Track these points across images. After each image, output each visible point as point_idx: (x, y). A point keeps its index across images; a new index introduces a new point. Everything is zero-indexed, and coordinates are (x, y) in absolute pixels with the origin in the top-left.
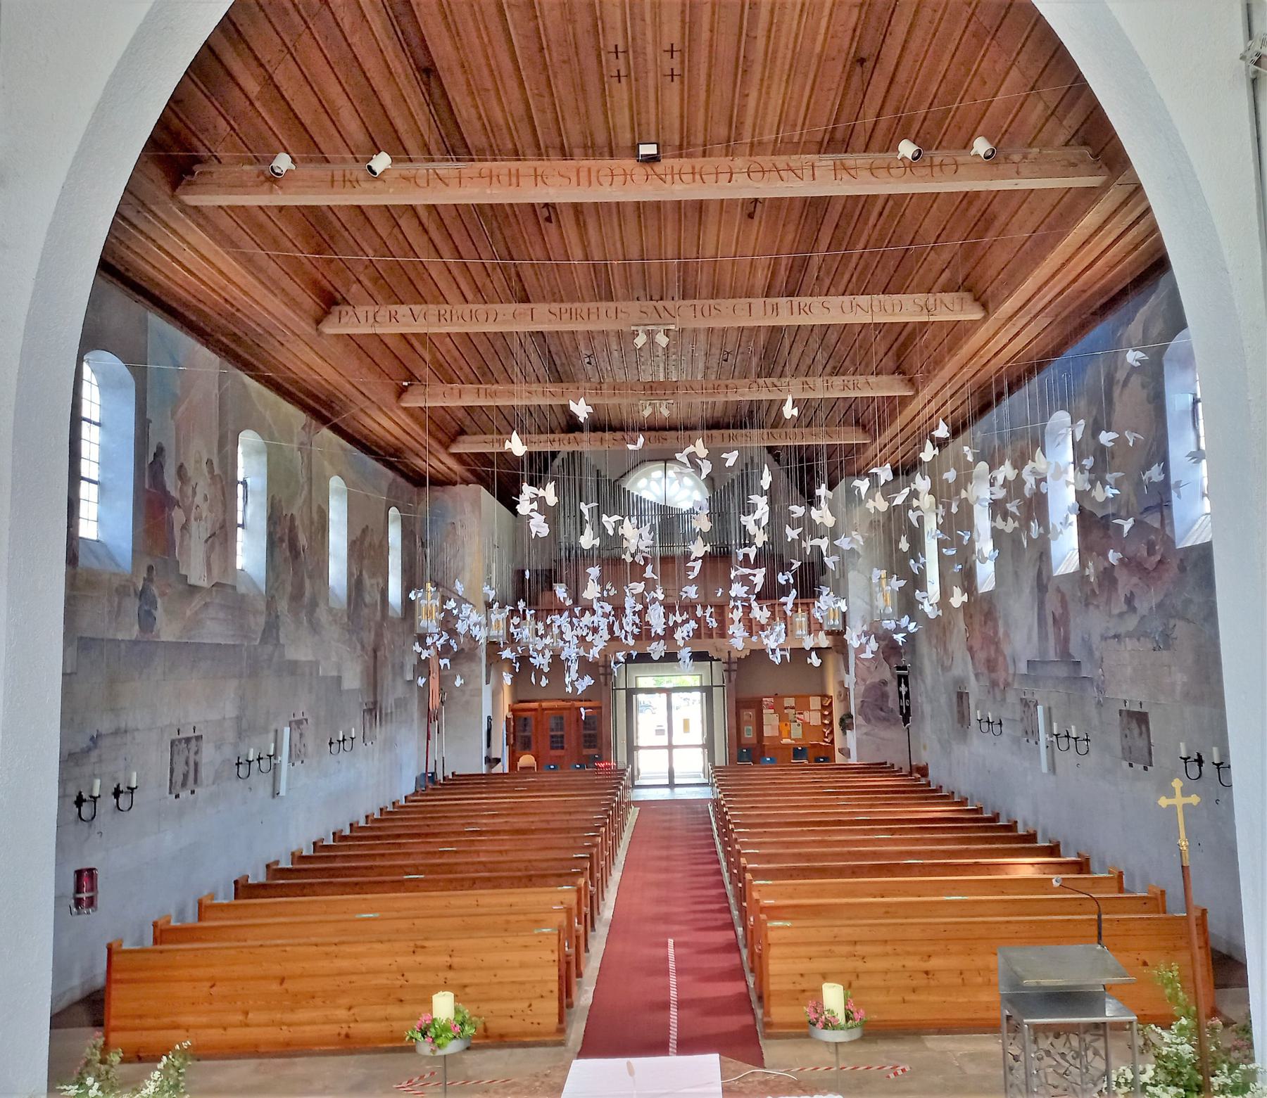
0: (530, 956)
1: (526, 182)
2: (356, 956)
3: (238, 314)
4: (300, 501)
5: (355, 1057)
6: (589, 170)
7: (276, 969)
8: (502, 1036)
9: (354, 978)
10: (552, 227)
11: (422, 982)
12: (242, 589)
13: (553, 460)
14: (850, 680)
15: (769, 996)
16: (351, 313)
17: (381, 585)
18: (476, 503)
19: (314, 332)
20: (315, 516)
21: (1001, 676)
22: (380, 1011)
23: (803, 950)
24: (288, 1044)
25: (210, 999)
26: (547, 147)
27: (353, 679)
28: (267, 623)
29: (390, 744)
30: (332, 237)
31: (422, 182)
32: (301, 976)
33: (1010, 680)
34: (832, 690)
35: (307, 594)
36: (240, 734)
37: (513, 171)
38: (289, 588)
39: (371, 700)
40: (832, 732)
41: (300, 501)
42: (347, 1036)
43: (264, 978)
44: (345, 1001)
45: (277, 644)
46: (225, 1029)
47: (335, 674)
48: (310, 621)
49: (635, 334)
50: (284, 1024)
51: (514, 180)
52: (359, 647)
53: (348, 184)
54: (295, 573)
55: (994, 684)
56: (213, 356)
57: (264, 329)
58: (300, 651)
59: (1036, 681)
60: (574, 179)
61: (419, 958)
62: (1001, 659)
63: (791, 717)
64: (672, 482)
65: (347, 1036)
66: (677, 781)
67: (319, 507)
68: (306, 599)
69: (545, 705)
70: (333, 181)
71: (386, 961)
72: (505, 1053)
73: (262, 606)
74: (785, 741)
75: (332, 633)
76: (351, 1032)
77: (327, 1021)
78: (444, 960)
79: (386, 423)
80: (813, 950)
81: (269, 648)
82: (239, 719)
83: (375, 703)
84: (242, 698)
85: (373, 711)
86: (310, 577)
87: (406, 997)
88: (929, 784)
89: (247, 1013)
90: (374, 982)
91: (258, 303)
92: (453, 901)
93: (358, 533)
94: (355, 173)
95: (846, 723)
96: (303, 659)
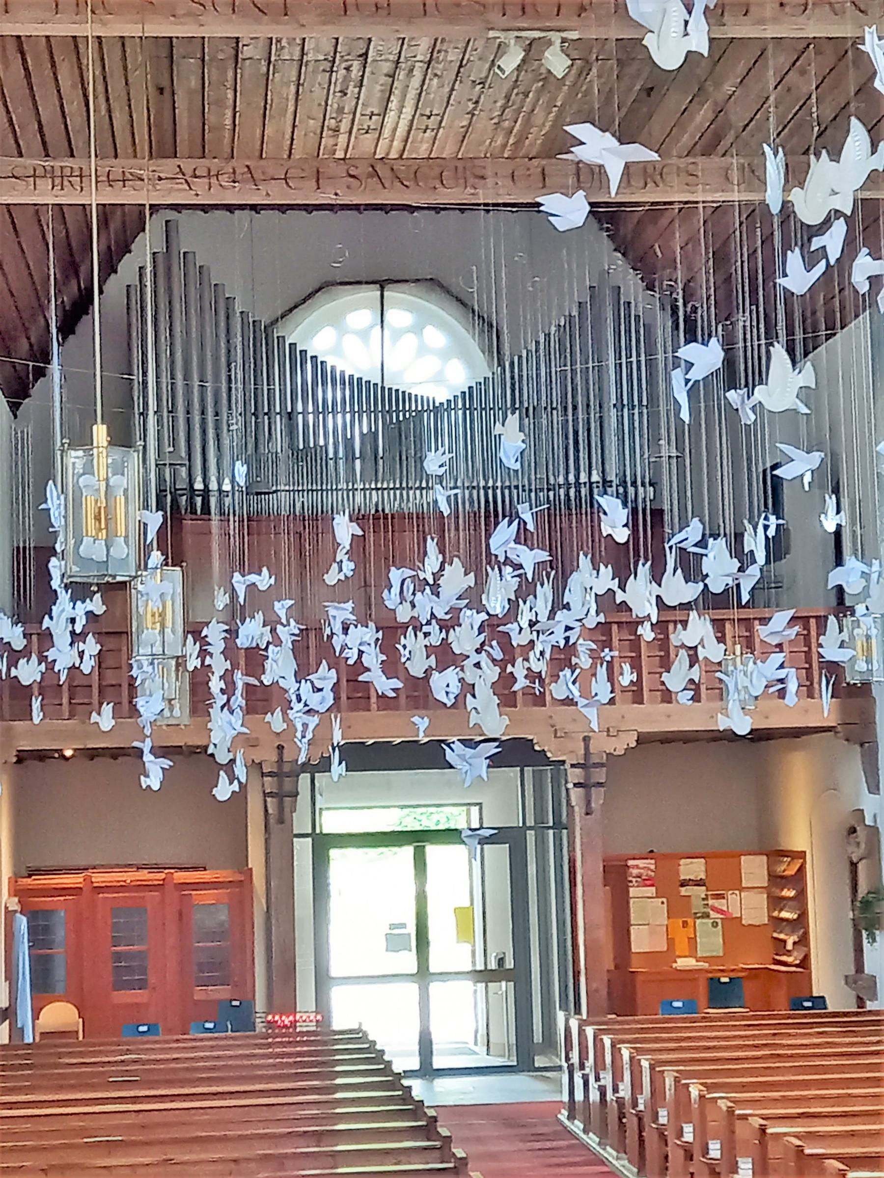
13: (109, 267)
34: (799, 835)
40: (803, 941)
63: (697, 906)
64: (398, 334)
66: (438, 1062)
69: (99, 878)
74: (683, 963)
88: (294, 1024)
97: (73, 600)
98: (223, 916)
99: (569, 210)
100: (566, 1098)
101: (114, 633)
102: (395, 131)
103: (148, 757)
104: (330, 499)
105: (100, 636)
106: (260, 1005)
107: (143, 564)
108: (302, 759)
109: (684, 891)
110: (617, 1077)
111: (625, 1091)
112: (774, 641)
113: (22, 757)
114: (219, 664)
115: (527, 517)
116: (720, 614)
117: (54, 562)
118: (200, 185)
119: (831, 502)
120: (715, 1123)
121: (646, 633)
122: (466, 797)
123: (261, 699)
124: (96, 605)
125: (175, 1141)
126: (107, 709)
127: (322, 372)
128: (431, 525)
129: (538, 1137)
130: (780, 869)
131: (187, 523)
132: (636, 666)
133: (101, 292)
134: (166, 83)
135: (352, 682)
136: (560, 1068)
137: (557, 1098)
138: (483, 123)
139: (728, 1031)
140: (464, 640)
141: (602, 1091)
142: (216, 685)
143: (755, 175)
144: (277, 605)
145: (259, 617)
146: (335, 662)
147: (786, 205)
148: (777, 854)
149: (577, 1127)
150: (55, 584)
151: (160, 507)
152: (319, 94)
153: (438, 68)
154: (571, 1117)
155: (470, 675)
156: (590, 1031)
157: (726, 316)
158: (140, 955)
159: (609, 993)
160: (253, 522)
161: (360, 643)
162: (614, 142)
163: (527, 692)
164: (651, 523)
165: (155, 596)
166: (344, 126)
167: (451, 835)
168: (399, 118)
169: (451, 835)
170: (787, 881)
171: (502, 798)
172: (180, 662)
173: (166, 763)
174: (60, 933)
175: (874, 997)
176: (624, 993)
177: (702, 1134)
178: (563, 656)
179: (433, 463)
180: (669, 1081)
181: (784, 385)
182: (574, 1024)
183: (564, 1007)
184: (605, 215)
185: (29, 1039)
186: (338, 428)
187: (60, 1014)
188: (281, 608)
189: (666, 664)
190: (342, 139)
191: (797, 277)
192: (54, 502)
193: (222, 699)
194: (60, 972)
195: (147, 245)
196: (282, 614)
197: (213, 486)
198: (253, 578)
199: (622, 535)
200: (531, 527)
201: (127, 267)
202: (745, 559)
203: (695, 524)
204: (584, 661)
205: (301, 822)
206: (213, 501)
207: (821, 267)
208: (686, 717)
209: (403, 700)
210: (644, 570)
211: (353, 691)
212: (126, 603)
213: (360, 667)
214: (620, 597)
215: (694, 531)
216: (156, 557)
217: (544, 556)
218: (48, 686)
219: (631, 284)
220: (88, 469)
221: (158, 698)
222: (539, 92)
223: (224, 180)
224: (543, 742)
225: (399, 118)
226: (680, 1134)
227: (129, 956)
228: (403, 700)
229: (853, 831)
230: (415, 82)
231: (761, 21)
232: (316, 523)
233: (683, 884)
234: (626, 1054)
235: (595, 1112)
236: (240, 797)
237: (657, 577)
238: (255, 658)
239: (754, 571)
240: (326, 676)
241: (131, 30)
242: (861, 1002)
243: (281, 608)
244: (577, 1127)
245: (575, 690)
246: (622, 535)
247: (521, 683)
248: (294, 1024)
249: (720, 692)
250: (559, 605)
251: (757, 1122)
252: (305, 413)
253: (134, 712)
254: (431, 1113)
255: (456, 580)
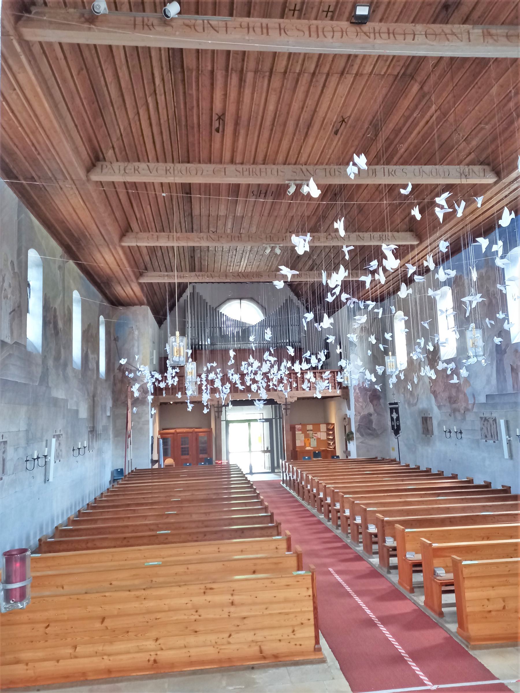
0: (291, 593)
1: (274, 33)
2: (160, 598)
3: (38, 157)
4: (59, 300)
5: (166, 680)
6: (317, 27)
7: (99, 611)
8: (276, 656)
9: (159, 616)
10: (217, 137)
11: (211, 616)
12: (29, 349)
13: (180, 296)
14: (351, 413)
15: (467, 616)
16: (109, 166)
17: (96, 359)
18: (145, 317)
19: (84, 178)
20: (66, 312)
21: (462, 405)
22: (180, 642)
23: (486, 582)
24: (109, 671)
25: (46, 637)
26: (232, 69)
27: (84, 413)
28: (43, 372)
29: (100, 452)
30: (104, 108)
31: (200, 29)
32: (118, 616)
33: (470, 407)
34: (333, 419)
35: (63, 357)
36: (28, 441)
37: (264, 25)
38: (53, 353)
39: (92, 425)
40: (334, 443)
41: (59, 300)
42: (155, 661)
43: (90, 618)
44: (154, 634)
45: (48, 387)
46: (58, 661)
47: (75, 408)
48: (64, 375)
49: (288, 186)
50: (105, 654)
51: (265, 31)
52: (86, 394)
53: (146, 27)
54: (57, 344)
55: (455, 410)
56: (14, 196)
57: (53, 175)
58: (59, 394)
59: (494, 406)
60: (307, 33)
61: (209, 598)
62: (461, 396)
63: (311, 436)
65: (155, 661)
67: (68, 306)
68: (62, 361)
70: (135, 25)
71: (184, 601)
72: (282, 670)
73: (40, 362)
74: (308, 448)
75: (74, 383)
76: (158, 658)
77: (140, 651)
78: (226, 598)
79: (108, 259)
80: (494, 581)
81: (44, 388)
82: (27, 431)
83: (93, 427)
84: (29, 418)
85: (93, 431)
86: (64, 348)
87: (200, 628)
88: (221, 463)
89: (75, 647)
90: (175, 618)
91: (54, 148)
92: (204, 549)
93: (86, 326)
94: (151, 20)
95: (349, 437)
96: (60, 397)
97: (172, 369)
98: (206, 438)
99: (279, 284)
100: (282, 479)
101: (181, 376)
102: (243, 266)
103: (189, 404)
104: (229, 346)
105: (179, 377)
106: (214, 458)
107: (187, 361)
108: (223, 404)
109: (308, 432)
110: (293, 474)
111: (295, 477)
112: (326, 378)
113: (161, 404)
114: (205, 383)
115: (272, 350)
116: (315, 371)
117: (168, 361)
118: (200, 278)
119: (338, 347)
120: (315, 484)
121: (299, 375)
122: (259, 411)
123: (214, 391)
124: (177, 370)
125: (195, 490)
126: (180, 393)
127: (228, 319)
128: (251, 352)
129: (276, 488)
130: (329, 427)
131: (198, 352)
132: (297, 382)
133: (178, 301)
134: (193, 255)
135: (234, 386)
136: (280, 472)
137: (279, 479)
138: (262, 264)
139: (319, 463)
140: (259, 377)
141: (290, 477)
142: (204, 388)
143: (320, 275)
144: (217, 370)
145: (213, 373)
146: (230, 382)
147: (327, 284)
148: (328, 424)
149: (284, 485)
150: (168, 366)
151: (192, 348)
152: (226, 258)
153: (253, 252)
154: (283, 483)
155: (260, 385)
156: (287, 464)
157: (314, 306)
158: (188, 448)
159: (292, 456)
160: (212, 352)
161: (236, 378)
162: (289, 270)
163: (273, 388)
164: (299, 352)
165: (190, 368)
166: (232, 265)
167: (256, 420)
168: (244, 263)
169: (256, 420)
170: (330, 430)
171: (266, 412)
172: (196, 383)
173: (193, 405)
174: (170, 443)
175: (350, 456)
176: (295, 455)
177: (312, 487)
178: (281, 381)
179: (252, 338)
180: (304, 475)
181: (327, 322)
182: (284, 462)
183: (281, 458)
184: (290, 285)
185: (162, 467)
186: (230, 330)
187: (170, 461)
188: (218, 370)
189: (303, 382)
190: (232, 268)
191: (330, 299)
192: (168, 348)
193: (205, 391)
194: (169, 451)
195: (189, 291)
196: (218, 372)
197: (203, 343)
198: (212, 364)
199: (293, 354)
200: (273, 353)
201: (185, 296)
202: (319, 360)
203: (309, 352)
204: (285, 381)
205: (223, 417)
206: (203, 347)
207: (335, 296)
208: (308, 394)
209: (245, 390)
210: (298, 362)
211: (234, 389)
212: (184, 369)
213: (235, 383)
214: (293, 368)
215: (308, 354)
216: (190, 360)
217: (276, 359)
218: (167, 388)
219: (295, 298)
220: (175, 341)
221: (191, 391)
222: (275, 257)
223: (206, 277)
224: (276, 399)
225: (244, 263)
226: (307, 487)
227: (185, 448)
228: (245, 390)
229: (345, 419)
230: (247, 255)
231: (321, 242)
232: (227, 351)
233: (308, 431)
234: (295, 469)
235: (288, 483)
236: (209, 413)
237: (300, 363)
238: (212, 382)
239: (321, 363)
240: (228, 385)
241: (185, 244)
242: (347, 457)
243: (218, 370)
244: (284, 485)
245: (283, 389)
246: (293, 354)
247: (271, 387)
248: (221, 463)
249: (315, 388)
250: (279, 369)
251: (324, 484)
252: (224, 327)
253: (186, 394)
254: (252, 483)
255: (256, 364)
